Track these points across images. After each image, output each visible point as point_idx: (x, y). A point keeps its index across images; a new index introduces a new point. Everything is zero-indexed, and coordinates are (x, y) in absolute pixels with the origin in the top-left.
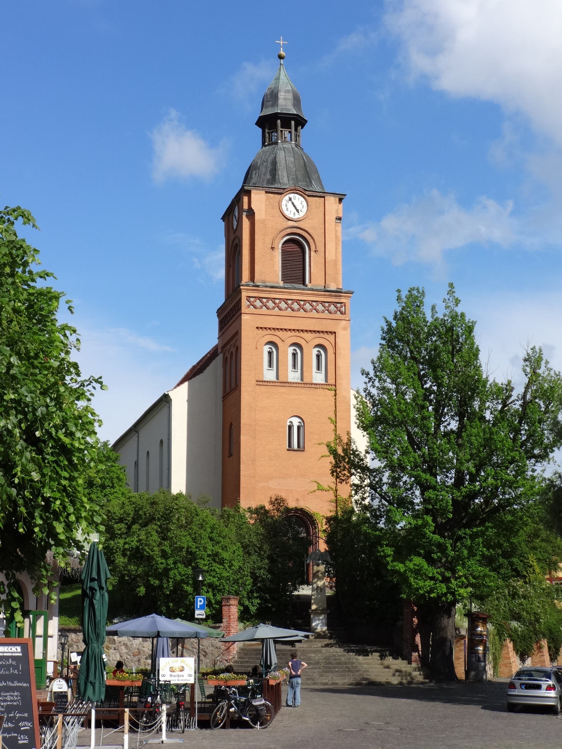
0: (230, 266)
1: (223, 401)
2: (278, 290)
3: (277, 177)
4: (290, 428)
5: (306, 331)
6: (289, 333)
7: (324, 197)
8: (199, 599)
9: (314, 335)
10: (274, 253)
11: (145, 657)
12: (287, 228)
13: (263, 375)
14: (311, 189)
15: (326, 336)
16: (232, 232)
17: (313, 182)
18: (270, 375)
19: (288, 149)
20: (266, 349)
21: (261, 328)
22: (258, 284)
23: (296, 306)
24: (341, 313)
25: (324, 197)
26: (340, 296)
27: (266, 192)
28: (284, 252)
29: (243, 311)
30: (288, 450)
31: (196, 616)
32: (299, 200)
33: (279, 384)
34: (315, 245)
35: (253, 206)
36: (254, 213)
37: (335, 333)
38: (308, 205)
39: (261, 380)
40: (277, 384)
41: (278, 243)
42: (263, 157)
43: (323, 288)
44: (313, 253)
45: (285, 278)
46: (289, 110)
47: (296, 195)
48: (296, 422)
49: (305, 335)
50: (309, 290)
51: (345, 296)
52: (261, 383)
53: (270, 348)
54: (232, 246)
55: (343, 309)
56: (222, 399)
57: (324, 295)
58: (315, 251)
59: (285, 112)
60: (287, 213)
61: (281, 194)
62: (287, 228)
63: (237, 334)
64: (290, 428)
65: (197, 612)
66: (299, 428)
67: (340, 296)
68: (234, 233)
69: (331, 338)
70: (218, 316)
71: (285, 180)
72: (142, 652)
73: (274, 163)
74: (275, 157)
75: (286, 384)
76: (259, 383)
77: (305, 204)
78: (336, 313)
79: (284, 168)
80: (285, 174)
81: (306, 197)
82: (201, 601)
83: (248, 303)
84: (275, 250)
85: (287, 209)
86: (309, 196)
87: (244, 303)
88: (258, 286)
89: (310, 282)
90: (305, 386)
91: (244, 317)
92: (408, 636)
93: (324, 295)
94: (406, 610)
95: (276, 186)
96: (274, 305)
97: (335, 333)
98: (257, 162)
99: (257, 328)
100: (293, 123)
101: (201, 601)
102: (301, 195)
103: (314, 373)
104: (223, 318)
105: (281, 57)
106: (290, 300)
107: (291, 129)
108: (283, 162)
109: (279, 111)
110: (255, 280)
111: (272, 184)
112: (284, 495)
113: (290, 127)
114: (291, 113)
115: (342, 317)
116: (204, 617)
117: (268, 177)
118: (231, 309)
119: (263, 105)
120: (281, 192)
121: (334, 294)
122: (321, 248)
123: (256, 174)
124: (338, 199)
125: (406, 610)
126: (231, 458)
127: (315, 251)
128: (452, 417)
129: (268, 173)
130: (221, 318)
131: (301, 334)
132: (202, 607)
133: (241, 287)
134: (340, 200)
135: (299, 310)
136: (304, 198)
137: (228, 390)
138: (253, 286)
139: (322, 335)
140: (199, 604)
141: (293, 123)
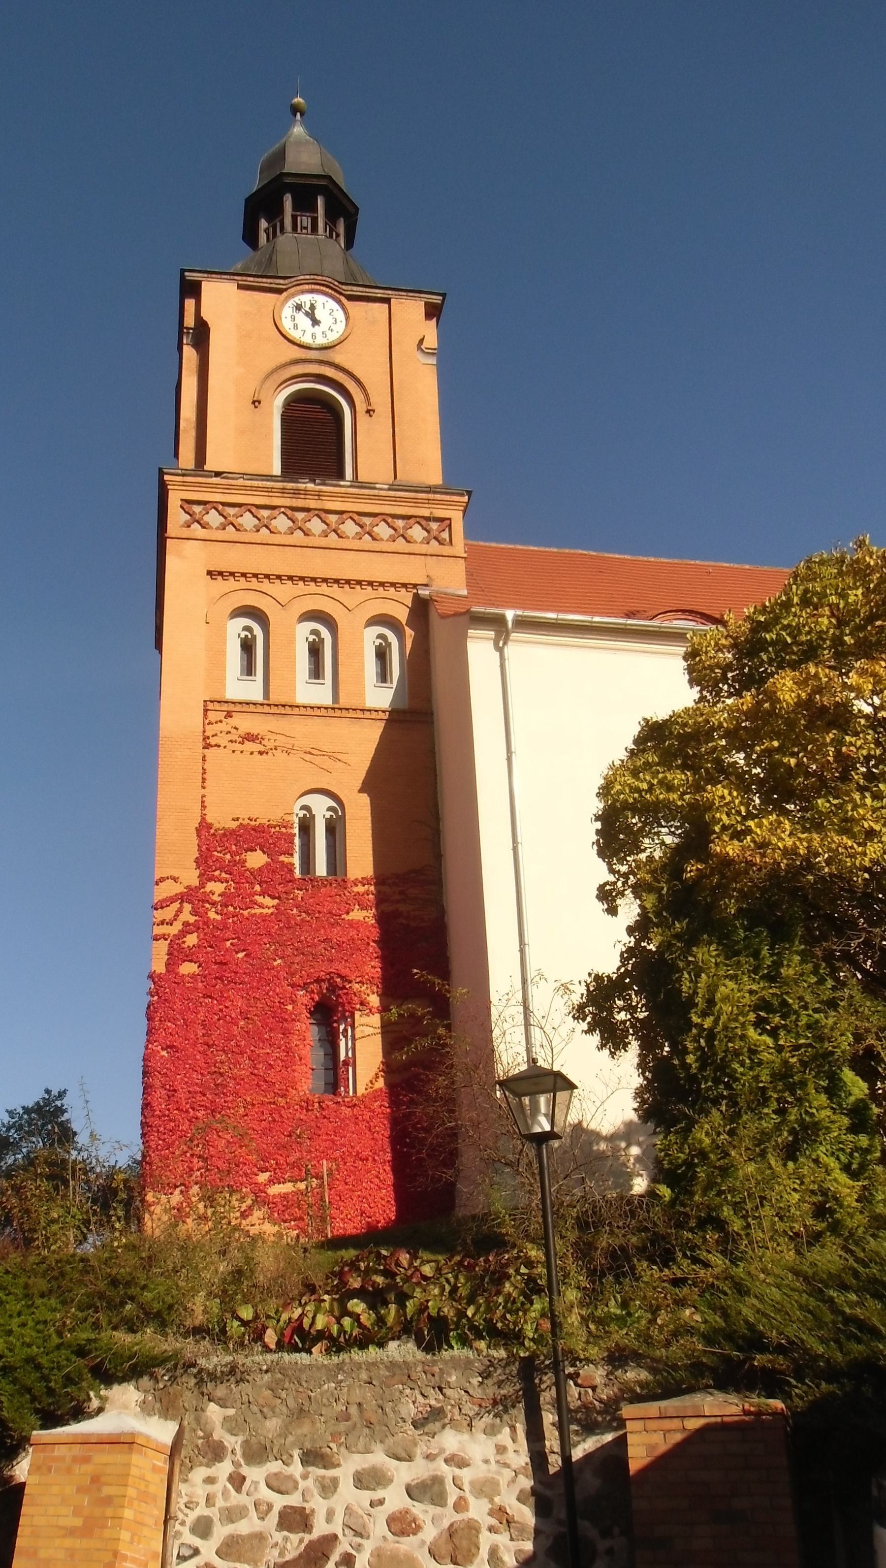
4: (306, 827)
5: (279, 577)
7: (387, 301)
13: (294, 691)
20: (304, 631)
27: (240, 287)
34: (367, 395)
35: (204, 314)
38: (347, 318)
48: (321, 806)
53: (315, 632)
55: (445, 535)
58: (368, 411)
60: (295, 335)
61: (279, 291)
77: (340, 315)
81: (343, 299)
85: (296, 327)
86: (351, 298)
99: (209, 573)
100: (320, 201)
115: (446, 550)
122: (380, 401)
127: (368, 411)
128: (801, 927)
131: (266, 586)
136: (339, 302)
141: (320, 201)
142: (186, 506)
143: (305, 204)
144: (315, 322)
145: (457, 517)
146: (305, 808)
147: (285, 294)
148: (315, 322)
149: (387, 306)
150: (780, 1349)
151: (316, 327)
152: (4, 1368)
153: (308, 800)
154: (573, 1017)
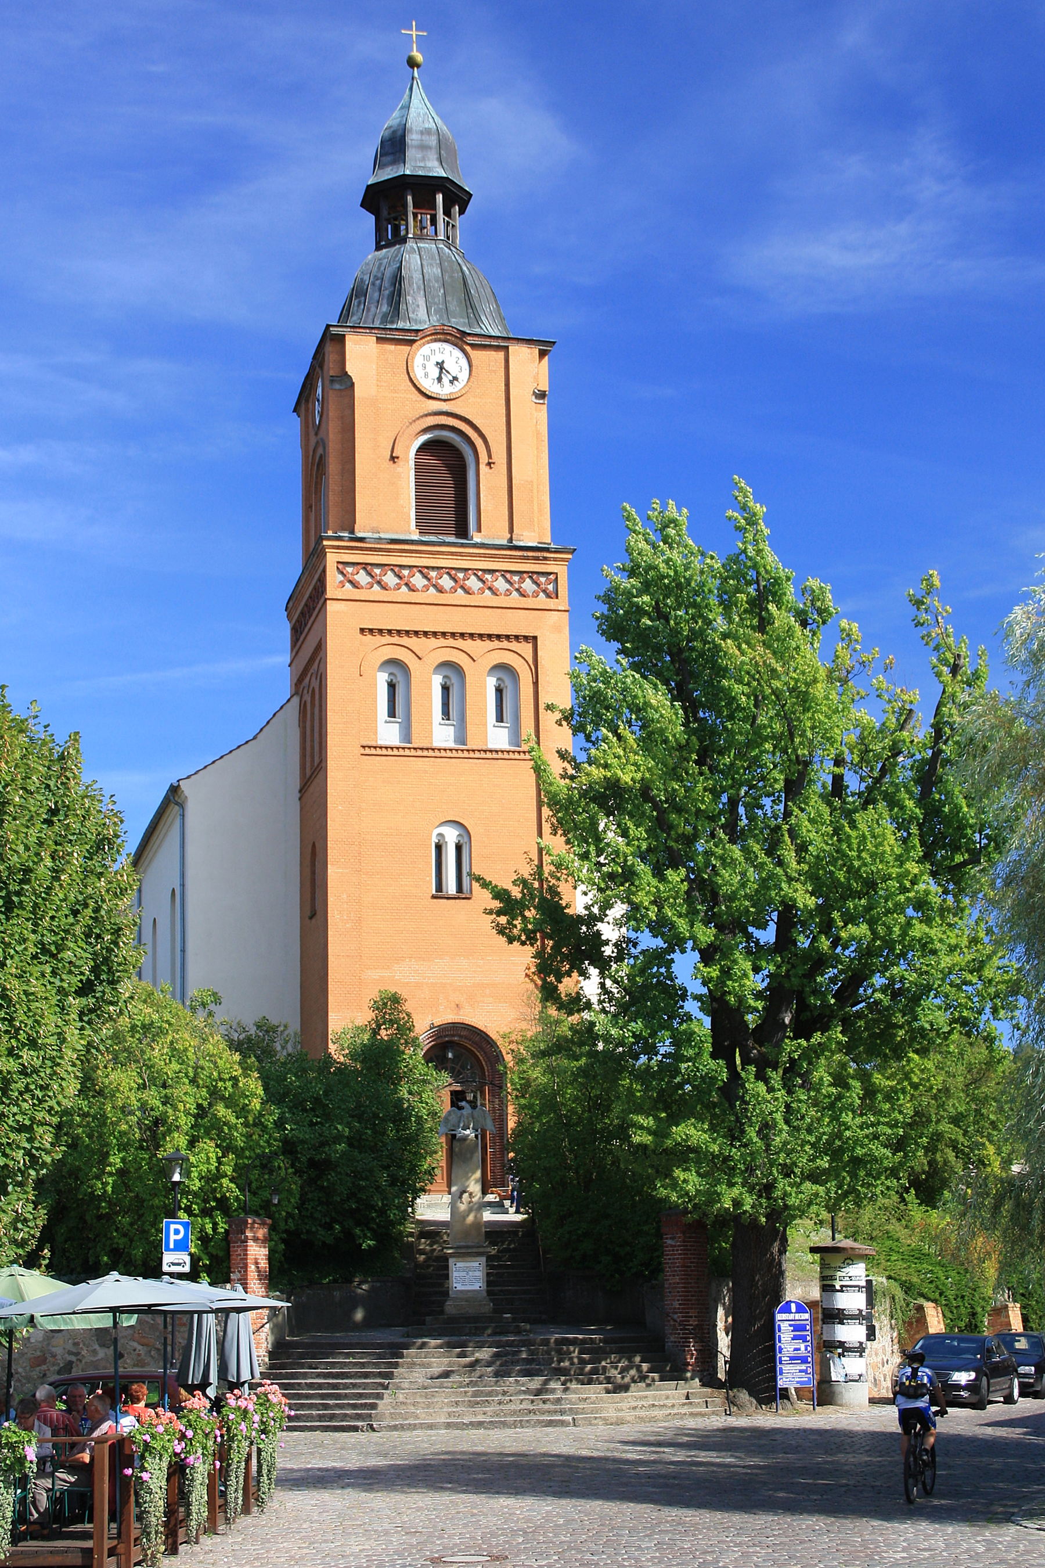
0: (311, 507)
1: (300, 799)
2: (407, 547)
3: (402, 307)
4: (439, 848)
6: (433, 642)
8: (173, 1227)
9: (488, 644)
10: (399, 470)
11: (56, 1368)
12: (426, 415)
13: (376, 733)
14: (478, 331)
15: (514, 645)
16: (312, 433)
17: (483, 318)
18: (389, 733)
19: (429, 251)
21: (371, 631)
22: (360, 535)
23: (446, 582)
24: (548, 596)
25: (507, 348)
26: (545, 559)
28: (419, 468)
29: (329, 595)
30: (434, 897)
31: (165, 1268)
32: (451, 356)
33: (413, 753)
36: (353, 384)
37: (535, 638)
38: (470, 366)
39: (374, 744)
40: (407, 752)
41: (408, 447)
42: (375, 269)
43: (505, 542)
44: (483, 468)
45: (424, 522)
46: (430, 169)
47: (446, 346)
48: (451, 836)
49: (467, 644)
50: (476, 546)
51: (555, 559)
52: (372, 749)
54: (313, 464)
56: (298, 795)
57: (511, 557)
58: (489, 464)
59: (420, 173)
61: (411, 342)
62: (426, 415)
63: (320, 647)
64: (439, 848)
65: (168, 1258)
66: (459, 848)
67: (545, 559)
68: (316, 434)
69: (526, 649)
70: (289, 617)
71: (422, 313)
72: (50, 1359)
73: (397, 279)
74: (400, 268)
75: (429, 751)
76: (367, 751)
78: (536, 595)
79: (419, 288)
80: (421, 302)
81: (468, 348)
82: (177, 1232)
83: (341, 578)
84: (400, 462)
86: (473, 346)
87: (333, 578)
88: (361, 540)
89: (479, 530)
90: (472, 755)
91: (331, 606)
92: (676, 1304)
93: (511, 557)
94: (669, 1242)
95: (401, 325)
96: (397, 581)
97: (535, 638)
98: (362, 279)
99: (362, 630)
100: (440, 198)
101: (177, 1232)
102: (456, 345)
103: (490, 728)
104: (298, 621)
105: (412, 63)
106: (433, 568)
107: (435, 209)
108: (417, 276)
109: (408, 172)
110: (356, 527)
111: (392, 322)
112: (403, 993)
113: (433, 206)
114: (435, 174)
115: (552, 603)
116: (187, 1269)
117: (385, 308)
118: (310, 597)
119: (379, 162)
120: (409, 339)
121: (530, 554)
123: (359, 305)
124: (537, 351)
125: (669, 1242)
126: (314, 920)
127: (489, 464)
129: (385, 301)
130: (294, 621)
132: (181, 1246)
133: (325, 543)
134: (542, 354)
135: (454, 590)
137: (308, 773)
138: (352, 539)
139: (505, 644)
140: (173, 1237)
141: (440, 198)
142: (340, 566)
143: (425, 203)
144: (441, 366)
145: (561, 570)
146: (440, 835)
147: (417, 344)
148: (441, 366)
149: (502, 353)
150: (780, 1261)
151: (440, 361)
152: (3, 706)
153: (442, 830)
154: (600, 626)
